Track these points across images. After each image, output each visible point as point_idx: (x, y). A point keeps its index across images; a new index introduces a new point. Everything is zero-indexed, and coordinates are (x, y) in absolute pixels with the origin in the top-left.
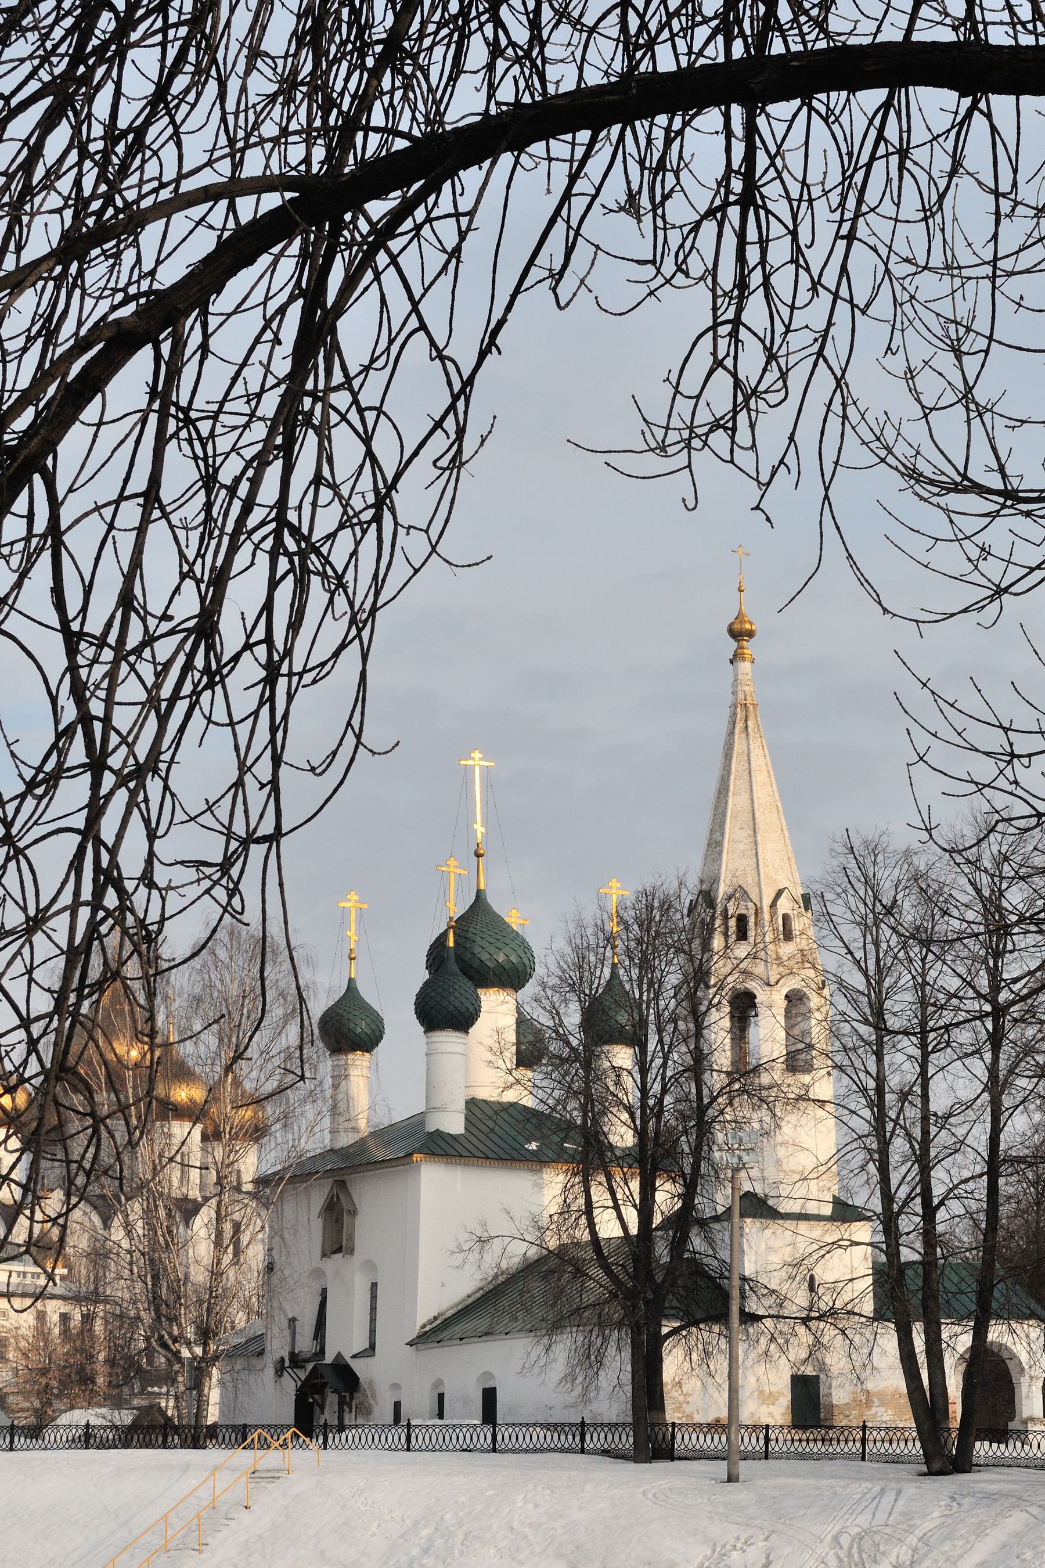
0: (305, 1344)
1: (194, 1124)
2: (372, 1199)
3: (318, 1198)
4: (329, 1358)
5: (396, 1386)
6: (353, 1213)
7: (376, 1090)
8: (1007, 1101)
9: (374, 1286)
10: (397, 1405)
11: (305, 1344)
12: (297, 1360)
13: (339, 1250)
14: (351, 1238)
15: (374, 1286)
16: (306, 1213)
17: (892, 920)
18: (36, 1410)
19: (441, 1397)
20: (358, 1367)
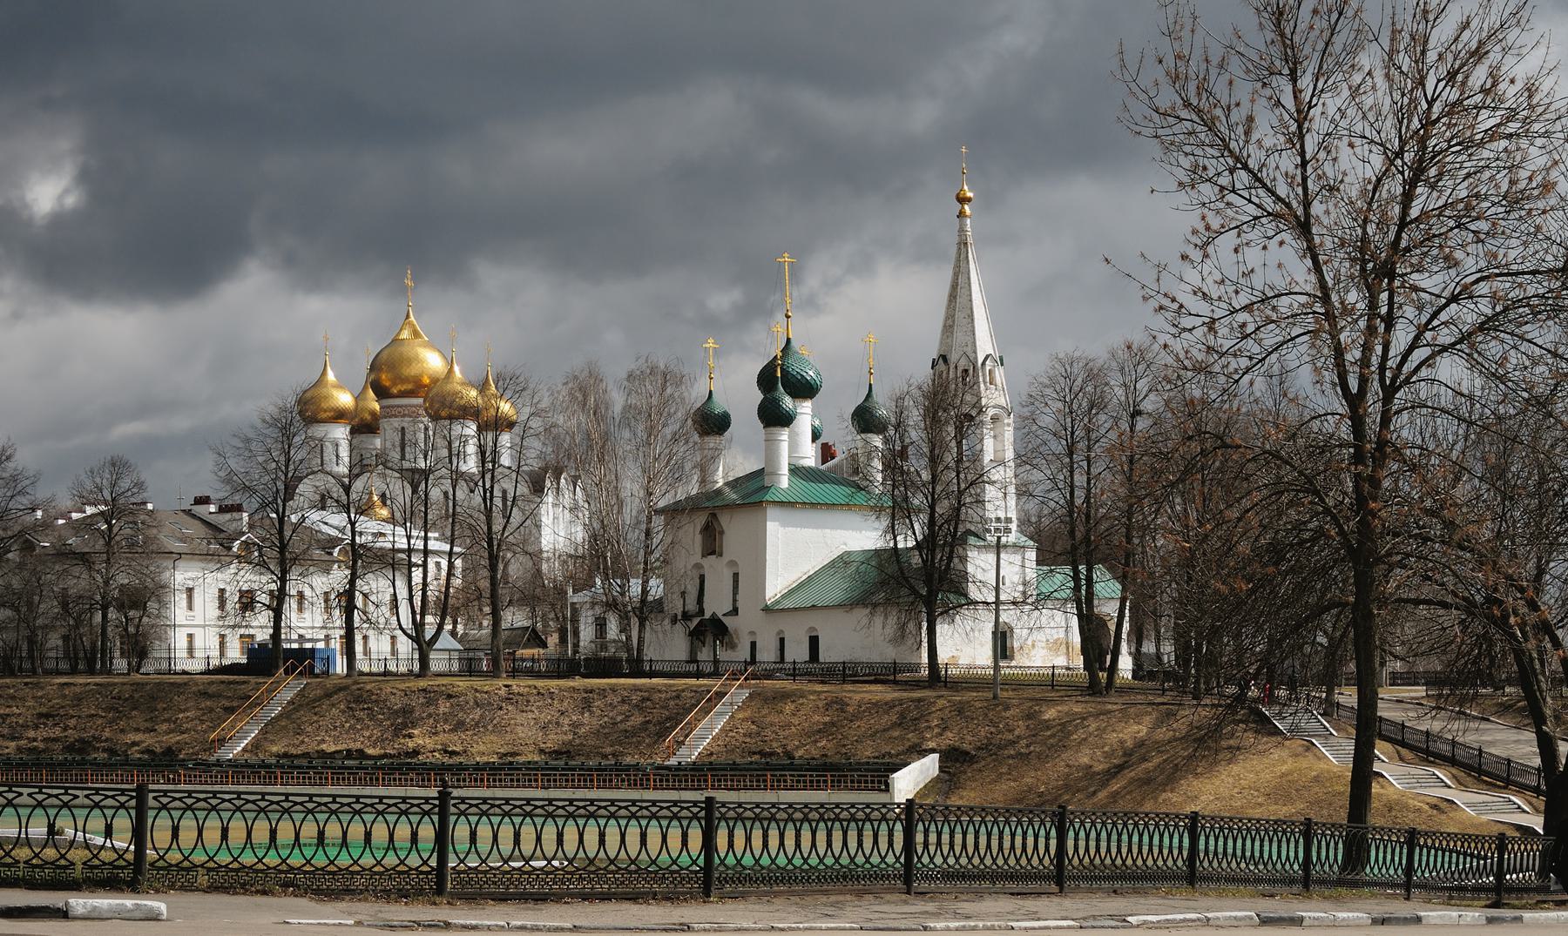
0: (692, 606)
1: (643, 601)
2: (733, 529)
3: (701, 520)
4: (707, 616)
5: (752, 633)
6: (722, 533)
7: (732, 462)
8: (1397, 403)
9: (736, 576)
10: (753, 644)
11: (692, 606)
12: (686, 616)
13: (713, 553)
14: (721, 546)
15: (736, 576)
16: (691, 533)
17: (1074, 416)
18: (480, 430)
19: (782, 641)
20: (727, 621)
